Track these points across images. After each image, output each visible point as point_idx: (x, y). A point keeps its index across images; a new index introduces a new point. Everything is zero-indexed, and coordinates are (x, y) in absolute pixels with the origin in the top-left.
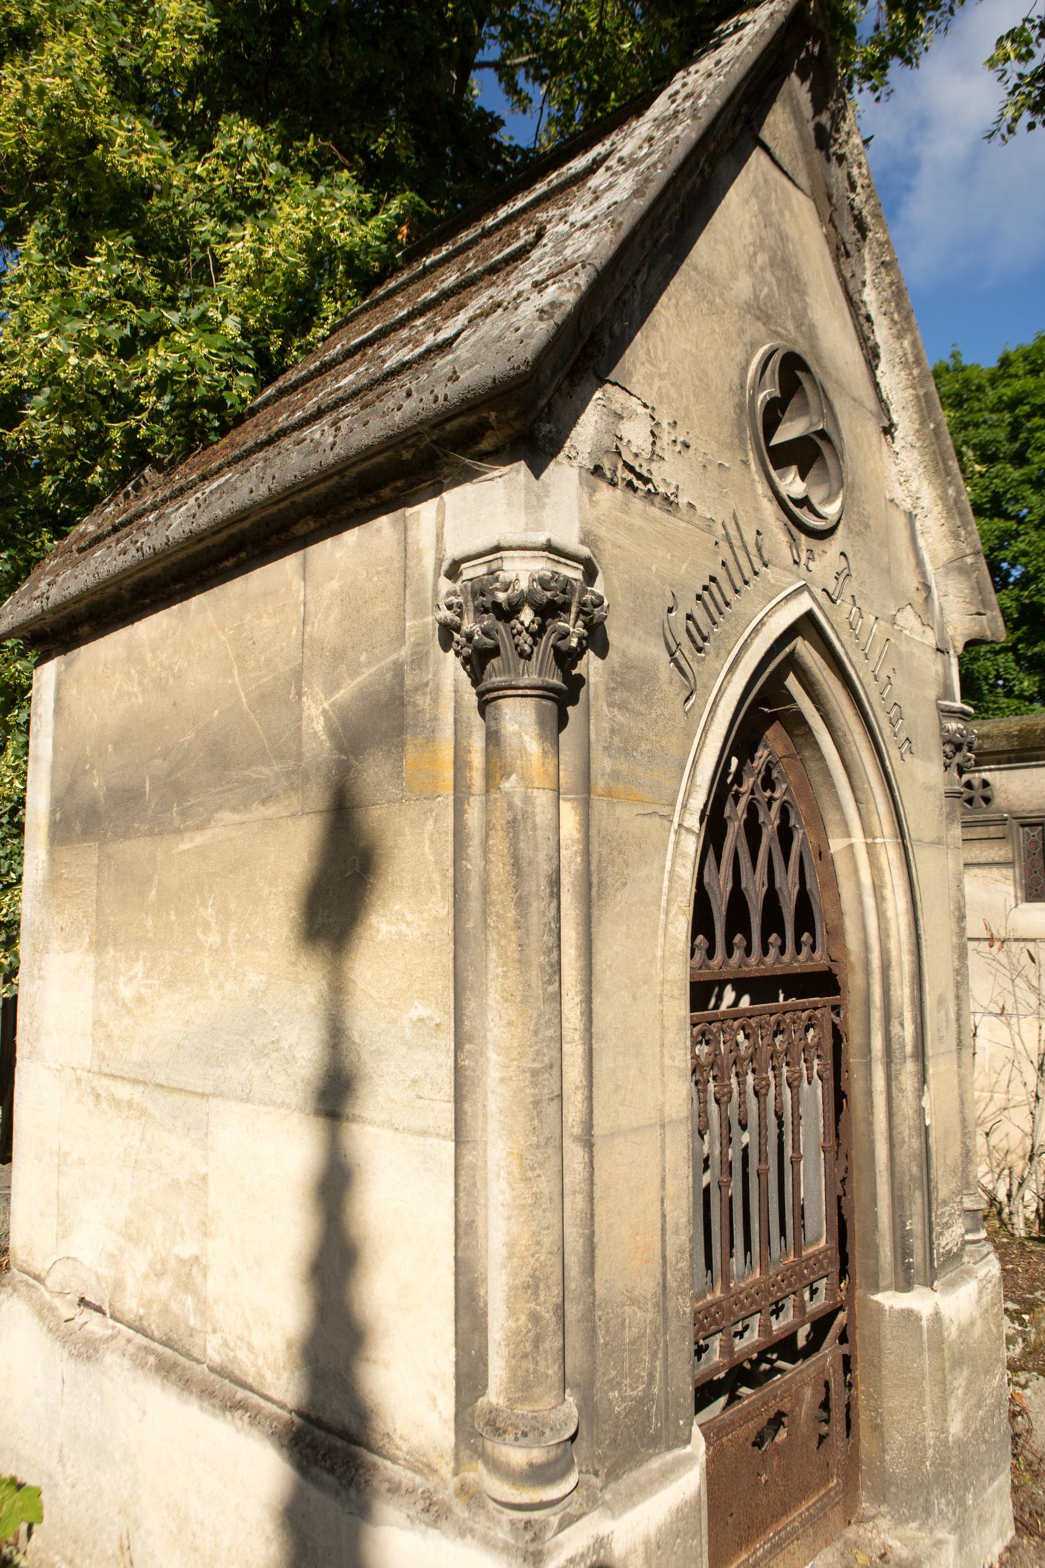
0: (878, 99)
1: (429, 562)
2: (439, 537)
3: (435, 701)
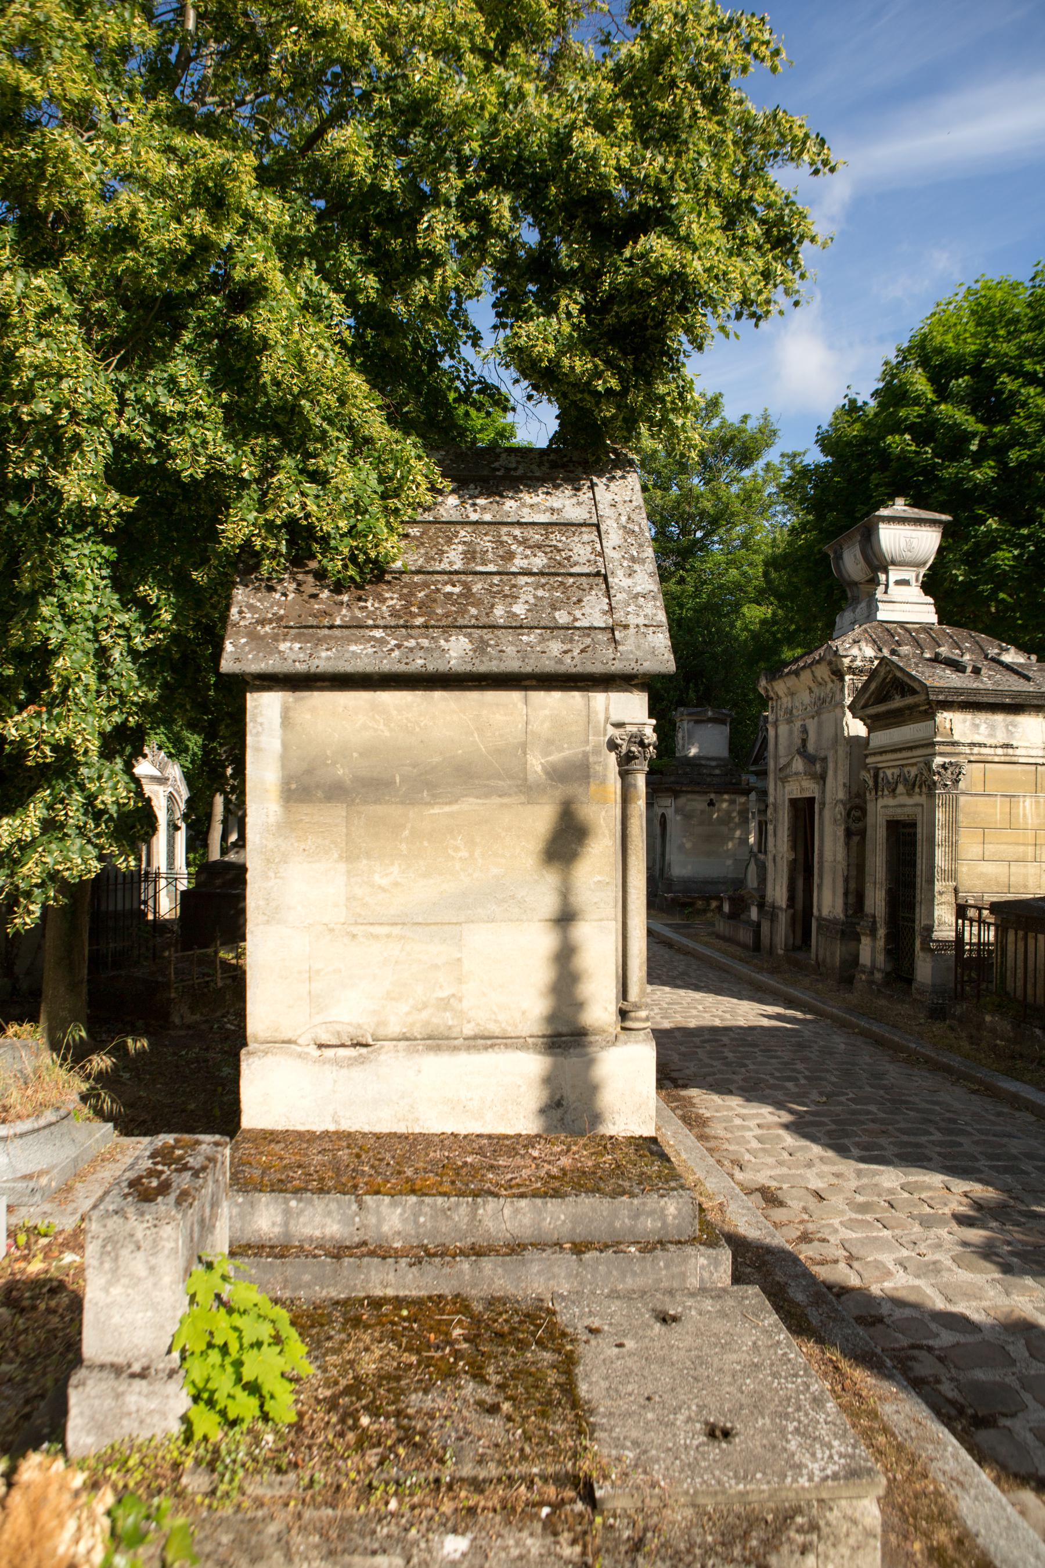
0: (737, 336)
1: (602, 717)
2: (607, 709)
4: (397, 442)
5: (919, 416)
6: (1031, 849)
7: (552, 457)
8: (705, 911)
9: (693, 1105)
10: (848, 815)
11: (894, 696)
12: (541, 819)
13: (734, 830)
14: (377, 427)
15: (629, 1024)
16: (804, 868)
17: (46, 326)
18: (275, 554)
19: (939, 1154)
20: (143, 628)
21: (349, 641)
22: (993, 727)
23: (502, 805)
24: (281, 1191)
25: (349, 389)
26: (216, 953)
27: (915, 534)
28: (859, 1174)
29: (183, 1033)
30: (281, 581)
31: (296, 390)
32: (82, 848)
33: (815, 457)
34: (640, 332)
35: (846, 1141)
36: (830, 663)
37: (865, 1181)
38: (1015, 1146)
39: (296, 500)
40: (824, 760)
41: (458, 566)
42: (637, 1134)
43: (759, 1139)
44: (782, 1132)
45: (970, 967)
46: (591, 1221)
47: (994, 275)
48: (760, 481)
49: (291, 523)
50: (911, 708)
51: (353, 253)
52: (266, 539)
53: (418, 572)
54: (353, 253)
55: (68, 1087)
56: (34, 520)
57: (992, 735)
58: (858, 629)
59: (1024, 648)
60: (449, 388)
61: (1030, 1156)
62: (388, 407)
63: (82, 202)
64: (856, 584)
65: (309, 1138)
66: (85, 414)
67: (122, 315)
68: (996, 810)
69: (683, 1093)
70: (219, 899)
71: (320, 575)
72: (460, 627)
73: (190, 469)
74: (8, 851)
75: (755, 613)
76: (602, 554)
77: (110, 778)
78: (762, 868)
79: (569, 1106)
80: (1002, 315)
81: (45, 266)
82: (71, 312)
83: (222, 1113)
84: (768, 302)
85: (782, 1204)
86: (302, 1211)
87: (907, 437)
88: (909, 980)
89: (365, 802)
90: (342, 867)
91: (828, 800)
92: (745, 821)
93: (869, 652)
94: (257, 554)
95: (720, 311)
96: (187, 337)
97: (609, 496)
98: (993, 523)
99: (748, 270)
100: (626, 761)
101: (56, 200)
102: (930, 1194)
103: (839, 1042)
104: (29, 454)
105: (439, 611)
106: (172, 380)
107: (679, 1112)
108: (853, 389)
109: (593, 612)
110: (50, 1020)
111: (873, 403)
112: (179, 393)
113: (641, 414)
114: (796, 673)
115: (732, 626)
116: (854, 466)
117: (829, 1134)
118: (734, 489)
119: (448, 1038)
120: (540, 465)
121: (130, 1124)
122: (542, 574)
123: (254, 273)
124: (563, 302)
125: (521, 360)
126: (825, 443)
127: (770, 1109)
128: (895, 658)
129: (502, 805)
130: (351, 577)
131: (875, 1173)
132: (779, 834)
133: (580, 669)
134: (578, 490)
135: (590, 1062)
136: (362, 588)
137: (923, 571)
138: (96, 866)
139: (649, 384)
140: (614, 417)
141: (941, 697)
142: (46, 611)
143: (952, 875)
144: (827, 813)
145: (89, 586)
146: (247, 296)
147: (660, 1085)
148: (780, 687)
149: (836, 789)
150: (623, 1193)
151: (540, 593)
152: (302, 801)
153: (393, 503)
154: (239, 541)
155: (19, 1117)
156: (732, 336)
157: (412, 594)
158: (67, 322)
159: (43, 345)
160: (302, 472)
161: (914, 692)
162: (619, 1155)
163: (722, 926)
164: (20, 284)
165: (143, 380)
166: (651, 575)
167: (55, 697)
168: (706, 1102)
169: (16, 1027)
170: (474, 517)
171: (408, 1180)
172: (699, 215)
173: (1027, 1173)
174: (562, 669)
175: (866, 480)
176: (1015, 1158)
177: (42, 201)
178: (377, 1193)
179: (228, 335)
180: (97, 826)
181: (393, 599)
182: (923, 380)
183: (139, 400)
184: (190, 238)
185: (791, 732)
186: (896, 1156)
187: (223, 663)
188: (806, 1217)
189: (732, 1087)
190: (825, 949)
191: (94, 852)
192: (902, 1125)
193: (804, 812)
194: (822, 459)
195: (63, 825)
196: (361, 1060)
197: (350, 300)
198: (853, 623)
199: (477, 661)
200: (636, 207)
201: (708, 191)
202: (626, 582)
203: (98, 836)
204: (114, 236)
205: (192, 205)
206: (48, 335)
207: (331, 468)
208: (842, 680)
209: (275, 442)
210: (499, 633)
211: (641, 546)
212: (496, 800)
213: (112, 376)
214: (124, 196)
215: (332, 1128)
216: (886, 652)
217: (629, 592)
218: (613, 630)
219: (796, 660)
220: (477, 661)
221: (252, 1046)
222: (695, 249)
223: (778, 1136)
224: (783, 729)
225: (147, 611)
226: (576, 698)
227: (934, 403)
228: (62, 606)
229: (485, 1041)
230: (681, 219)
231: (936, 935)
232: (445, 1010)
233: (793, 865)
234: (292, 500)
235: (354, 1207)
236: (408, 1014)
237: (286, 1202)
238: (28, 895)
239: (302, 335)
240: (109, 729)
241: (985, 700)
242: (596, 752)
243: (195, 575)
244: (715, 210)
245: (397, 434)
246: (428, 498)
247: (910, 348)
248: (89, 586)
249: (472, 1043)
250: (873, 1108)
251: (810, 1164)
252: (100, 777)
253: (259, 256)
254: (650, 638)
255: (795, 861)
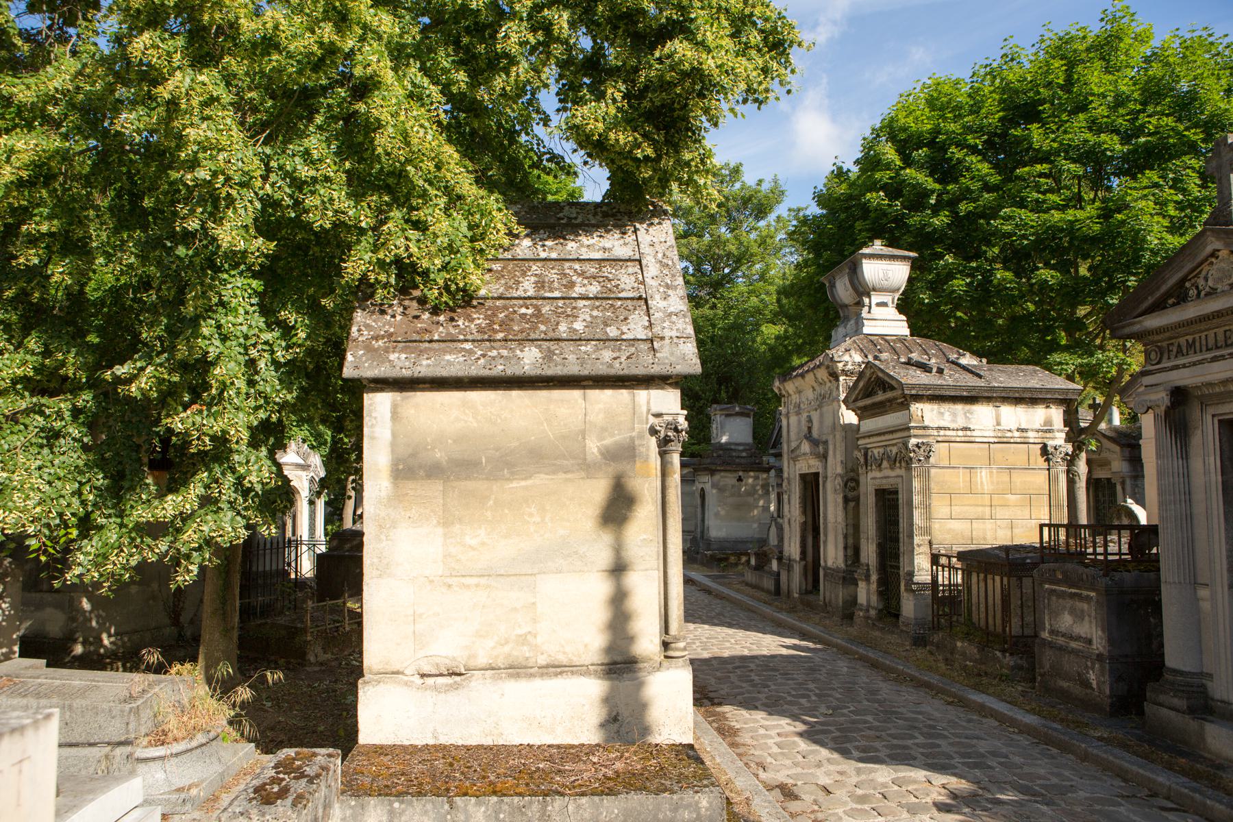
0: (743, 116)
1: (644, 409)
2: (648, 403)
3: (648, 450)
4: (482, 198)
5: (891, 178)
6: (988, 509)
7: (605, 208)
8: (736, 565)
9: (726, 719)
10: (846, 485)
11: (877, 392)
12: (597, 491)
13: (759, 500)
14: (467, 186)
15: (670, 653)
16: (812, 529)
17: (207, 112)
18: (386, 286)
19: (922, 754)
20: (284, 344)
21: (445, 352)
22: (954, 415)
23: (567, 480)
24: (387, 795)
25: (444, 158)
26: (344, 603)
27: (889, 267)
28: (858, 771)
29: (317, 669)
30: (391, 306)
31: (403, 159)
32: (232, 519)
33: (814, 210)
34: (668, 115)
35: (848, 745)
36: (828, 367)
37: (863, 777)
38: (983, 746)
39: (402, 241)
40: (826, 442)
41: (531, 293)
42: (678, 742)
43: (779, 745)
44: (797, 739)
45: (946, 604)
46: (639, 814)
47: (941, 75)
48: (772, 229)
49: (398, 261)
50: (890, 401)
51: (448, 55)
52: (378, 274)
53: (500, 298)
54: (448, 55)
55: (218, 714)
56: (197, 260)
57: (953, 421)
58: (849, 341)
59: (978, 354)
60: (525, 158)
61: (994, 754)
62: (476, 171)
63: (237, 18)
64: (846, 306)
65: (412, 750)
66: (237, 179)
67: (270, 103)
68: (959, 479)
69: (719, 709)
70: (344, 561)
71: (422, 301)
72: (532, 340)
73: (320, 221)
74: (172, 522)
75: (771, 331)
76: (643, 283)
77: (256, 462)
78: (780, 529)
79: (624, 721)
80: (949, 102)
81: (208, 66)
82: (228, 100)
83: (339, 729)
84: (767, 90)
85: (796, 798)
86: (404, 811)
87: (882, 194)
88: (897, 616)
89: (458, 479)
90: (440, 530)
91: (829, 474)
92: (767, 493)
93: (858, 358)
94: (372, 285)
95: (730, 97)
96: (319, 119)
97: (648, 238)
98: (949, 258)
99: (751, 67)
100: (664, 443)
101: (217, 16)
102: (915, 787)
103: (843, 666)
104: (192, 211)
105: (516, 328)
106: (307, 153)
107: (715, 725)
108: (840, 159)
109: (636, 327)
110: (206, 659)
111: (855, 169)
112: (312, 162)
113: (671, 175)
114: (802, 376)
115: (754, 341)
116: (843, 216)
117: (834, 739)
118: (753, 236)
119: (526, 667)
120: (595, 214)
121: (267, 745)
122: (597, 298)
123: (369, 71)
124: (610, 91)
125: (578, 134)
126: (821, 199)
127: (788, 721)
128: (877, 362)
129: (567, 480)
130: (446, 303)
131: (871, 771)
132: (792, 502)
133: (626, 372)
134: (624, 233)
135: (640, 685)
136: (454, 311)
137: (897, 296)
138: (244, 533)
139: (677, 152)
140: (651, 178)
141: (913, 392)
142: (205, 331)
143: (927, 531)
144: (829, 485)
145: (241, 311)
146: (364, 88)
147: (698, 702)
148: (790, 387)
149: (835, 465)
150: (665, 791)
151: (595, 313)
152: (407, 479)
153: (479, 245)
154: (357, 276)
155: (175, 740)
156: (739, 115)
157: (494, 315)
158: (224, 108)
159: (204, 126)
160: (407, 221)
161: (892, 388)
162: (662, 760)
163: (750, 576)
164: (188, 80)
165: (284, 152)
166: (681, 298)
167: (214, 398)
168: (736, 716)
169: (179, 666)
170: (543, 255)
171: (491, 783)
172: (712, 25)
173: (990, 767)
174: (612, 372)
175: (852, 226)
176: (983, 756)
177: (206, 17)
178: (465, 794)
179: (350, 118)
180: (245, 500)
181: (479, 319)
182: (893, 151)
183: (281, 168)
184: (321, 44)
185: (799, 421)
186: (889, 756)
187: (345, 370)
188: (816, 808)
189: (758, 704)
190: (832, 593)
191: (243, 522)
192: (893, 731)
193: (811, 484)
194: (818, 211)
195: (217, 501)
196: (456, 687)
197: (446, 90)
198: (845, 336)
199: (545, 367)
200: (663, 20)
201: (719, 9)
202: (662, 304)
203: (246, 509)
204: (262, 43)
205: (324, 20)
206: (208, 118)
207: (430, 218)
208: (837, 380)
209: (386, 198)
210: (562, 344)
211: (673, 276)
212: (562, 476)
213: (260, 150)
214: (269, 13)
215: (431, 742)
216: (870, 358)
217: (664, 312)
218: (652, 341)
219: (802, 365)
220: (545, 367)
221: (367, 677)
222: (709, 51)
223: (794, 742)
224: (793, 419)
225: (287, 331)
226: (624, 394)
227: (901, 168)
228: (219, 327)
229: (555, 669)
230: (698, 29)
231: (916, 579)
232: (523, 644)
233: (804, 526)
234: (398, 243)
235: (447, 807)
236: (493, 648)
237: (391, 804)
238: (188, 557)
239: (407, 117)
240: (255, 423)
241: (948, 393)
242: (641, 436)
243: (323, 302)
244: (726, 23)
245: (483, 192)
246: (506, 242)
247: (881, 128)
248: (241, 311)
249: (545, 670)
250: (869, 718)
251: (819, 765)
252: (248, 462)
253: (374, 58)
254: (681, 346)
255: (805, 523)
